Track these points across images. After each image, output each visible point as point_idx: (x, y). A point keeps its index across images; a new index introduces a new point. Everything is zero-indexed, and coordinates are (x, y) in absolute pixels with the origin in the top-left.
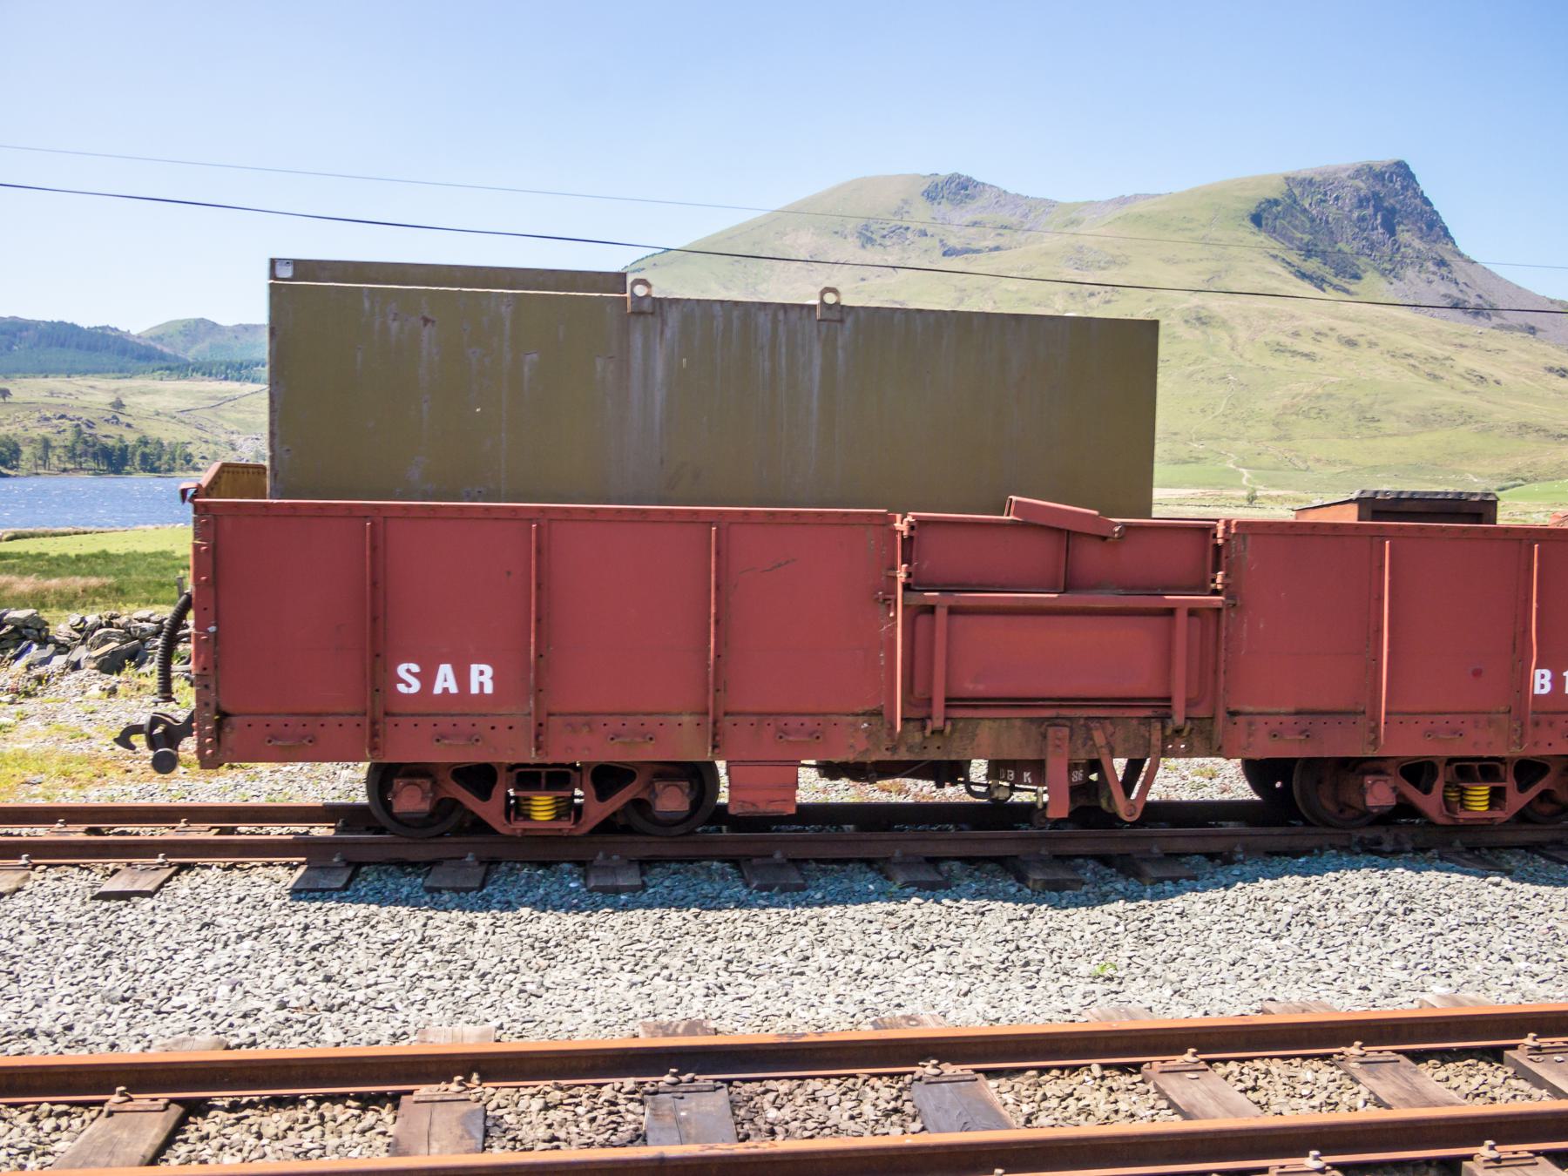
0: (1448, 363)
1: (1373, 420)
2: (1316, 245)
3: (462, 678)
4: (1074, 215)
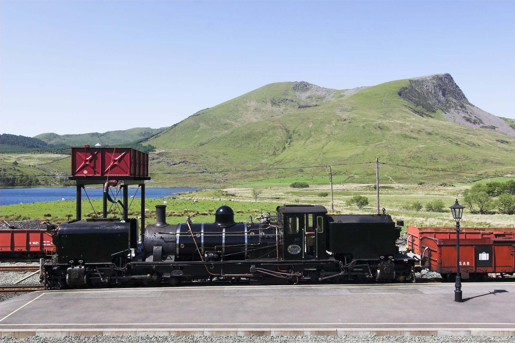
0: (462, 140)
1: (435, 159)
2: (420, 102)
3: (466, 263)
4: (342, 94)
